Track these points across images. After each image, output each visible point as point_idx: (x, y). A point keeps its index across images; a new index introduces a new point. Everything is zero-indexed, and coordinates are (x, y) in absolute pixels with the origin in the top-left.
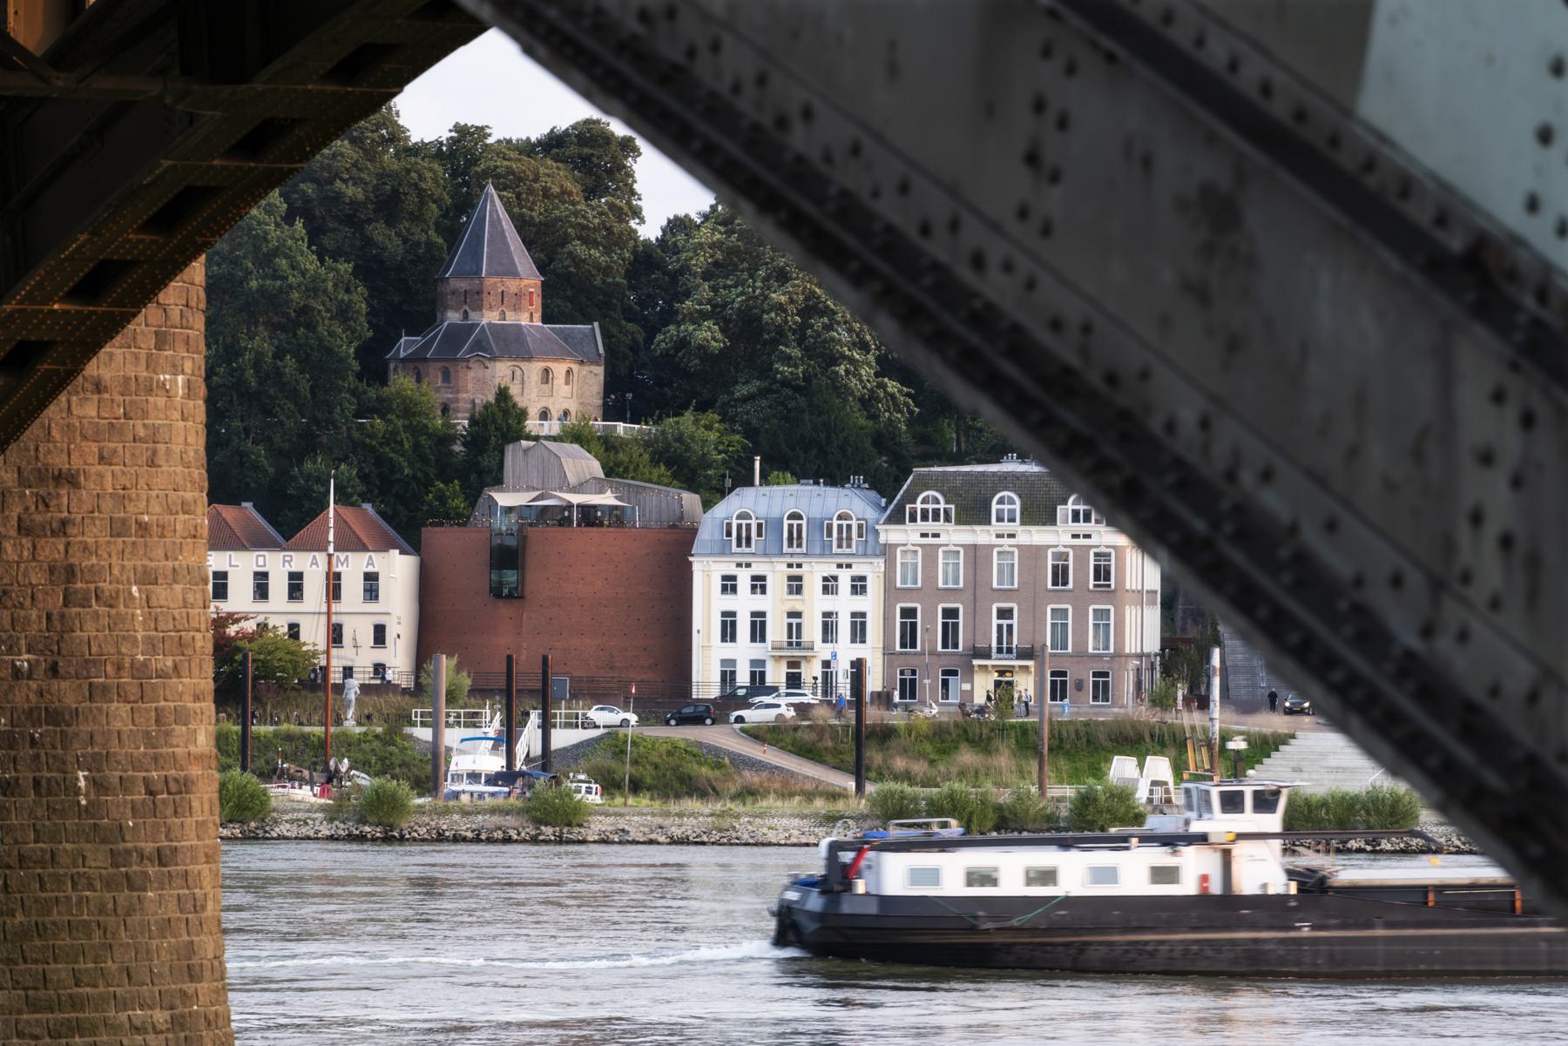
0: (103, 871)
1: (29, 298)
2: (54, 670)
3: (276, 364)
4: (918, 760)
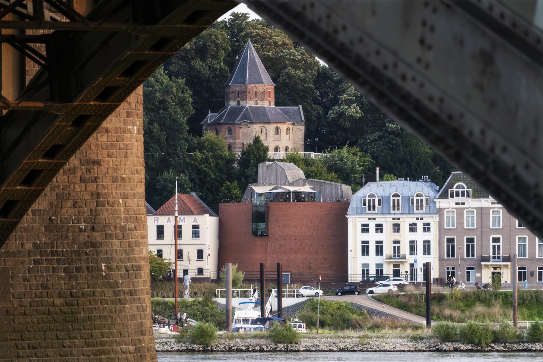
0: (111, 298)
1: (82, 100)
2: (93, 229)
3: (149, 127)
4: (456, 310)
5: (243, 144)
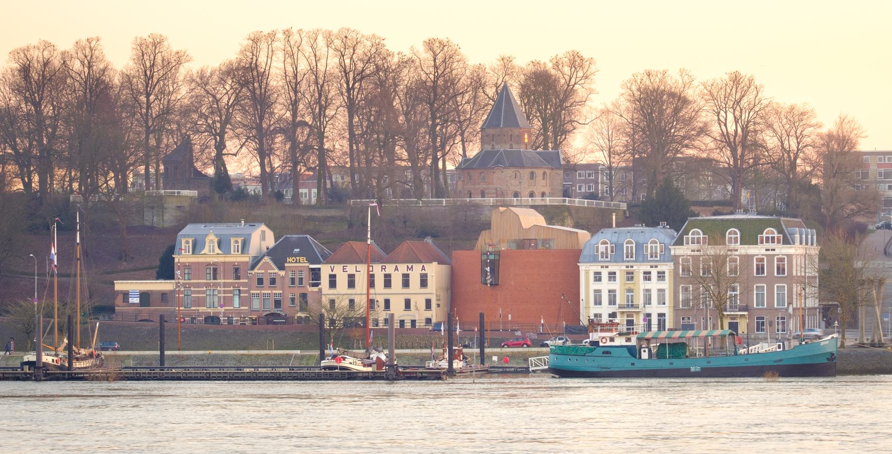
5: (496, 189)
